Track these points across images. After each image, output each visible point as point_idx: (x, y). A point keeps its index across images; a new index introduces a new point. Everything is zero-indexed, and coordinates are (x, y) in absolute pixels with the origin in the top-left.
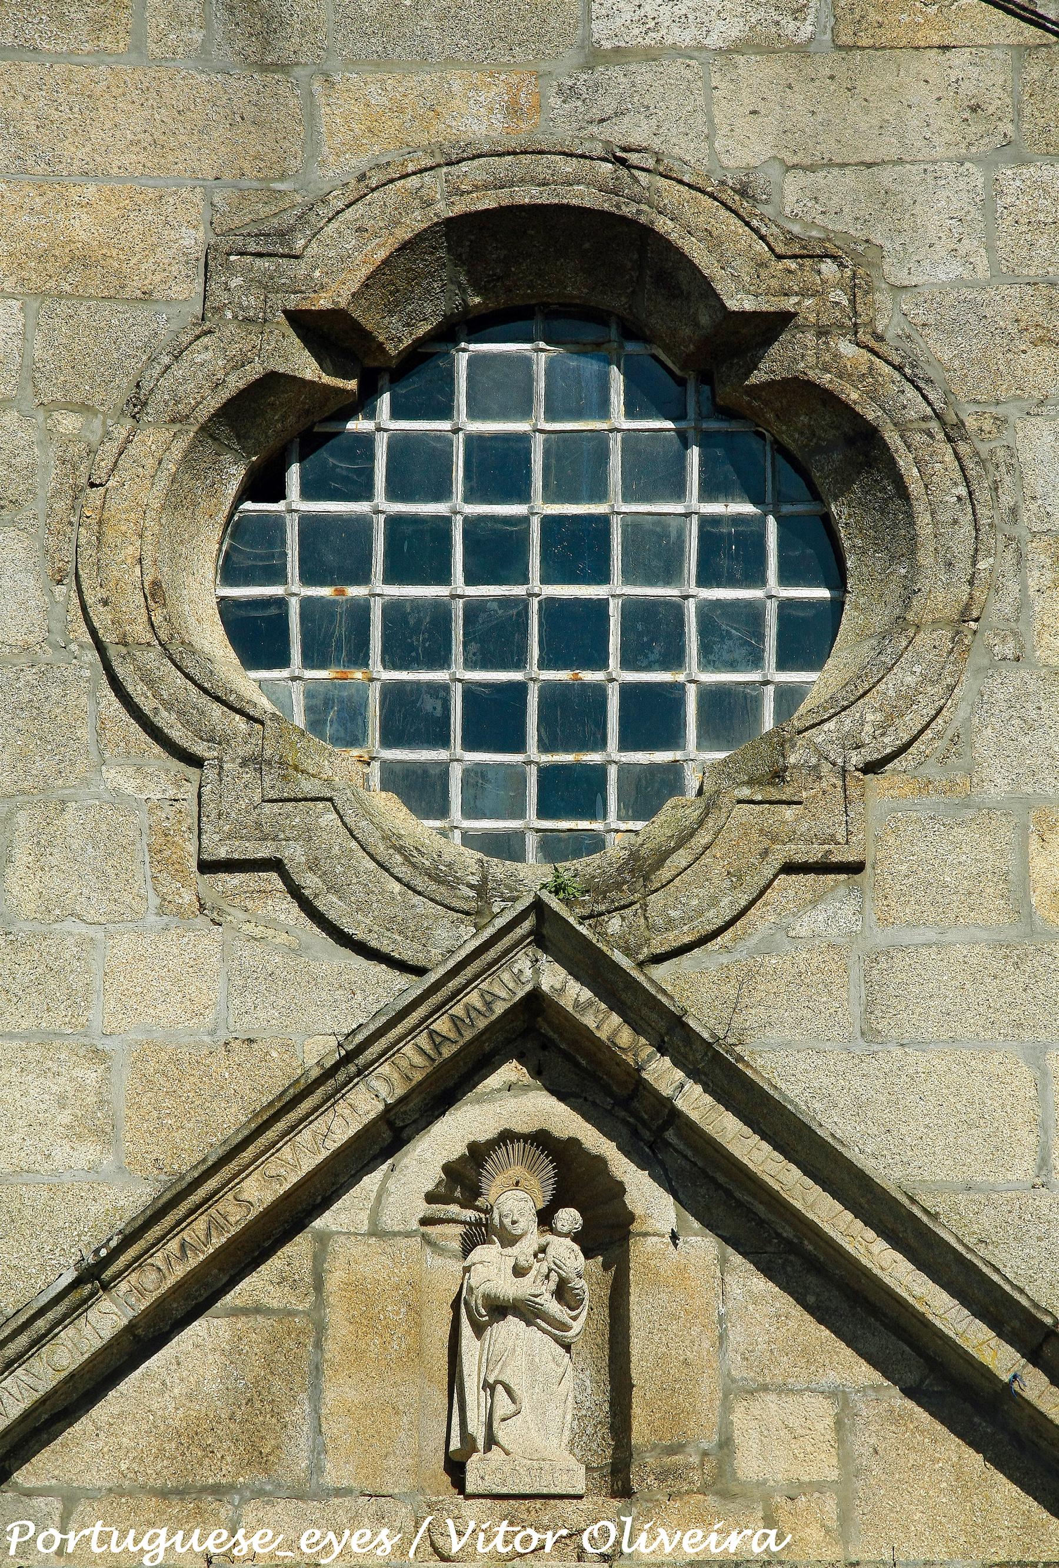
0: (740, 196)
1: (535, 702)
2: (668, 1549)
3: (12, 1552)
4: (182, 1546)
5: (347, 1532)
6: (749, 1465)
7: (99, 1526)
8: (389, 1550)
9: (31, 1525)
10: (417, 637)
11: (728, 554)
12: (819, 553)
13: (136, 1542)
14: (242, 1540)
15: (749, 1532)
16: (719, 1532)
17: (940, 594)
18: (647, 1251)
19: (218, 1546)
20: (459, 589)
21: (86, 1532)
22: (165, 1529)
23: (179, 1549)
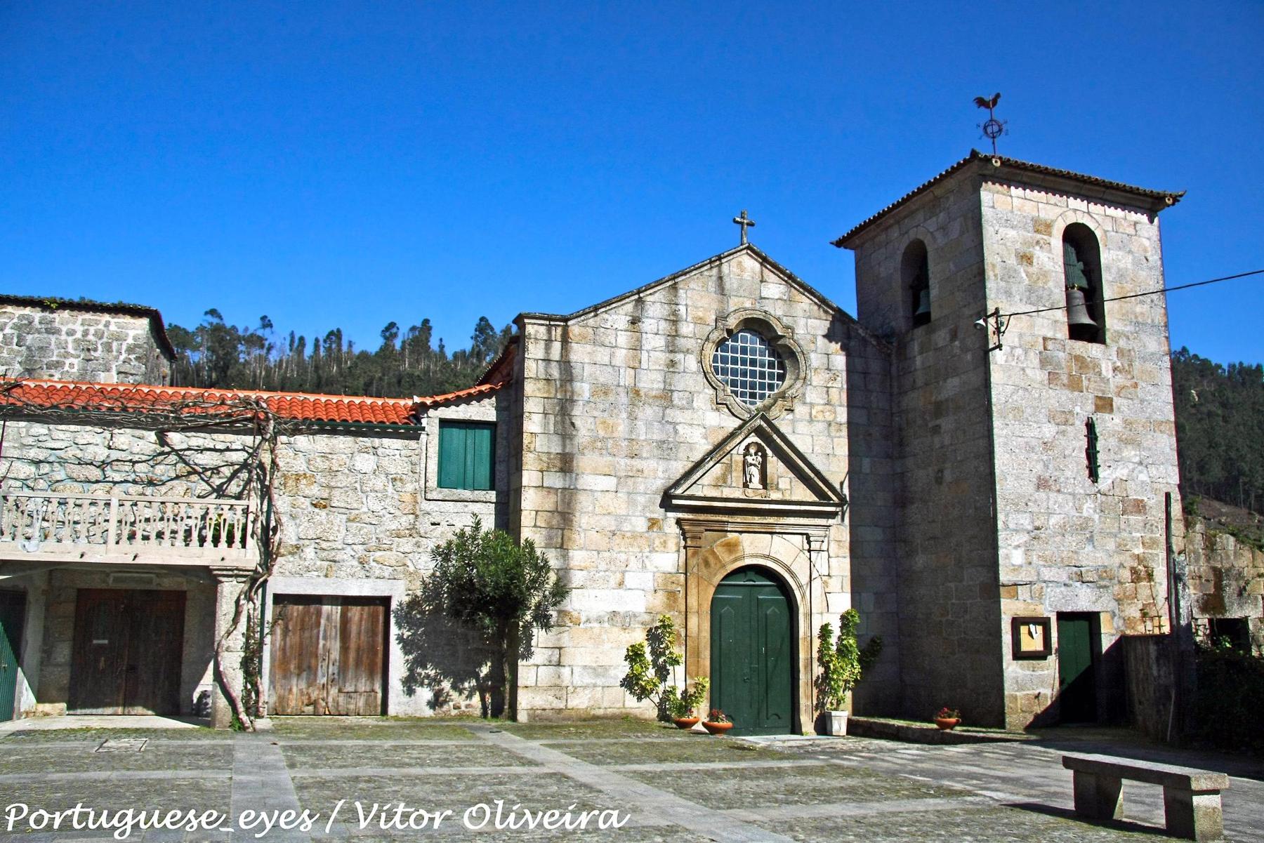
0: (778, 319)
3: (10, 828)
6: (780, 486)
7: (78, 809)
9: (25, 807)
11: (771, 365)
14: (193, 819)
15: (596, 812)
16: (573, 812)
17: (802, 375)
18: (769, 459)
20: (739, 366)
21: (69, 812)
23: (142, 825)
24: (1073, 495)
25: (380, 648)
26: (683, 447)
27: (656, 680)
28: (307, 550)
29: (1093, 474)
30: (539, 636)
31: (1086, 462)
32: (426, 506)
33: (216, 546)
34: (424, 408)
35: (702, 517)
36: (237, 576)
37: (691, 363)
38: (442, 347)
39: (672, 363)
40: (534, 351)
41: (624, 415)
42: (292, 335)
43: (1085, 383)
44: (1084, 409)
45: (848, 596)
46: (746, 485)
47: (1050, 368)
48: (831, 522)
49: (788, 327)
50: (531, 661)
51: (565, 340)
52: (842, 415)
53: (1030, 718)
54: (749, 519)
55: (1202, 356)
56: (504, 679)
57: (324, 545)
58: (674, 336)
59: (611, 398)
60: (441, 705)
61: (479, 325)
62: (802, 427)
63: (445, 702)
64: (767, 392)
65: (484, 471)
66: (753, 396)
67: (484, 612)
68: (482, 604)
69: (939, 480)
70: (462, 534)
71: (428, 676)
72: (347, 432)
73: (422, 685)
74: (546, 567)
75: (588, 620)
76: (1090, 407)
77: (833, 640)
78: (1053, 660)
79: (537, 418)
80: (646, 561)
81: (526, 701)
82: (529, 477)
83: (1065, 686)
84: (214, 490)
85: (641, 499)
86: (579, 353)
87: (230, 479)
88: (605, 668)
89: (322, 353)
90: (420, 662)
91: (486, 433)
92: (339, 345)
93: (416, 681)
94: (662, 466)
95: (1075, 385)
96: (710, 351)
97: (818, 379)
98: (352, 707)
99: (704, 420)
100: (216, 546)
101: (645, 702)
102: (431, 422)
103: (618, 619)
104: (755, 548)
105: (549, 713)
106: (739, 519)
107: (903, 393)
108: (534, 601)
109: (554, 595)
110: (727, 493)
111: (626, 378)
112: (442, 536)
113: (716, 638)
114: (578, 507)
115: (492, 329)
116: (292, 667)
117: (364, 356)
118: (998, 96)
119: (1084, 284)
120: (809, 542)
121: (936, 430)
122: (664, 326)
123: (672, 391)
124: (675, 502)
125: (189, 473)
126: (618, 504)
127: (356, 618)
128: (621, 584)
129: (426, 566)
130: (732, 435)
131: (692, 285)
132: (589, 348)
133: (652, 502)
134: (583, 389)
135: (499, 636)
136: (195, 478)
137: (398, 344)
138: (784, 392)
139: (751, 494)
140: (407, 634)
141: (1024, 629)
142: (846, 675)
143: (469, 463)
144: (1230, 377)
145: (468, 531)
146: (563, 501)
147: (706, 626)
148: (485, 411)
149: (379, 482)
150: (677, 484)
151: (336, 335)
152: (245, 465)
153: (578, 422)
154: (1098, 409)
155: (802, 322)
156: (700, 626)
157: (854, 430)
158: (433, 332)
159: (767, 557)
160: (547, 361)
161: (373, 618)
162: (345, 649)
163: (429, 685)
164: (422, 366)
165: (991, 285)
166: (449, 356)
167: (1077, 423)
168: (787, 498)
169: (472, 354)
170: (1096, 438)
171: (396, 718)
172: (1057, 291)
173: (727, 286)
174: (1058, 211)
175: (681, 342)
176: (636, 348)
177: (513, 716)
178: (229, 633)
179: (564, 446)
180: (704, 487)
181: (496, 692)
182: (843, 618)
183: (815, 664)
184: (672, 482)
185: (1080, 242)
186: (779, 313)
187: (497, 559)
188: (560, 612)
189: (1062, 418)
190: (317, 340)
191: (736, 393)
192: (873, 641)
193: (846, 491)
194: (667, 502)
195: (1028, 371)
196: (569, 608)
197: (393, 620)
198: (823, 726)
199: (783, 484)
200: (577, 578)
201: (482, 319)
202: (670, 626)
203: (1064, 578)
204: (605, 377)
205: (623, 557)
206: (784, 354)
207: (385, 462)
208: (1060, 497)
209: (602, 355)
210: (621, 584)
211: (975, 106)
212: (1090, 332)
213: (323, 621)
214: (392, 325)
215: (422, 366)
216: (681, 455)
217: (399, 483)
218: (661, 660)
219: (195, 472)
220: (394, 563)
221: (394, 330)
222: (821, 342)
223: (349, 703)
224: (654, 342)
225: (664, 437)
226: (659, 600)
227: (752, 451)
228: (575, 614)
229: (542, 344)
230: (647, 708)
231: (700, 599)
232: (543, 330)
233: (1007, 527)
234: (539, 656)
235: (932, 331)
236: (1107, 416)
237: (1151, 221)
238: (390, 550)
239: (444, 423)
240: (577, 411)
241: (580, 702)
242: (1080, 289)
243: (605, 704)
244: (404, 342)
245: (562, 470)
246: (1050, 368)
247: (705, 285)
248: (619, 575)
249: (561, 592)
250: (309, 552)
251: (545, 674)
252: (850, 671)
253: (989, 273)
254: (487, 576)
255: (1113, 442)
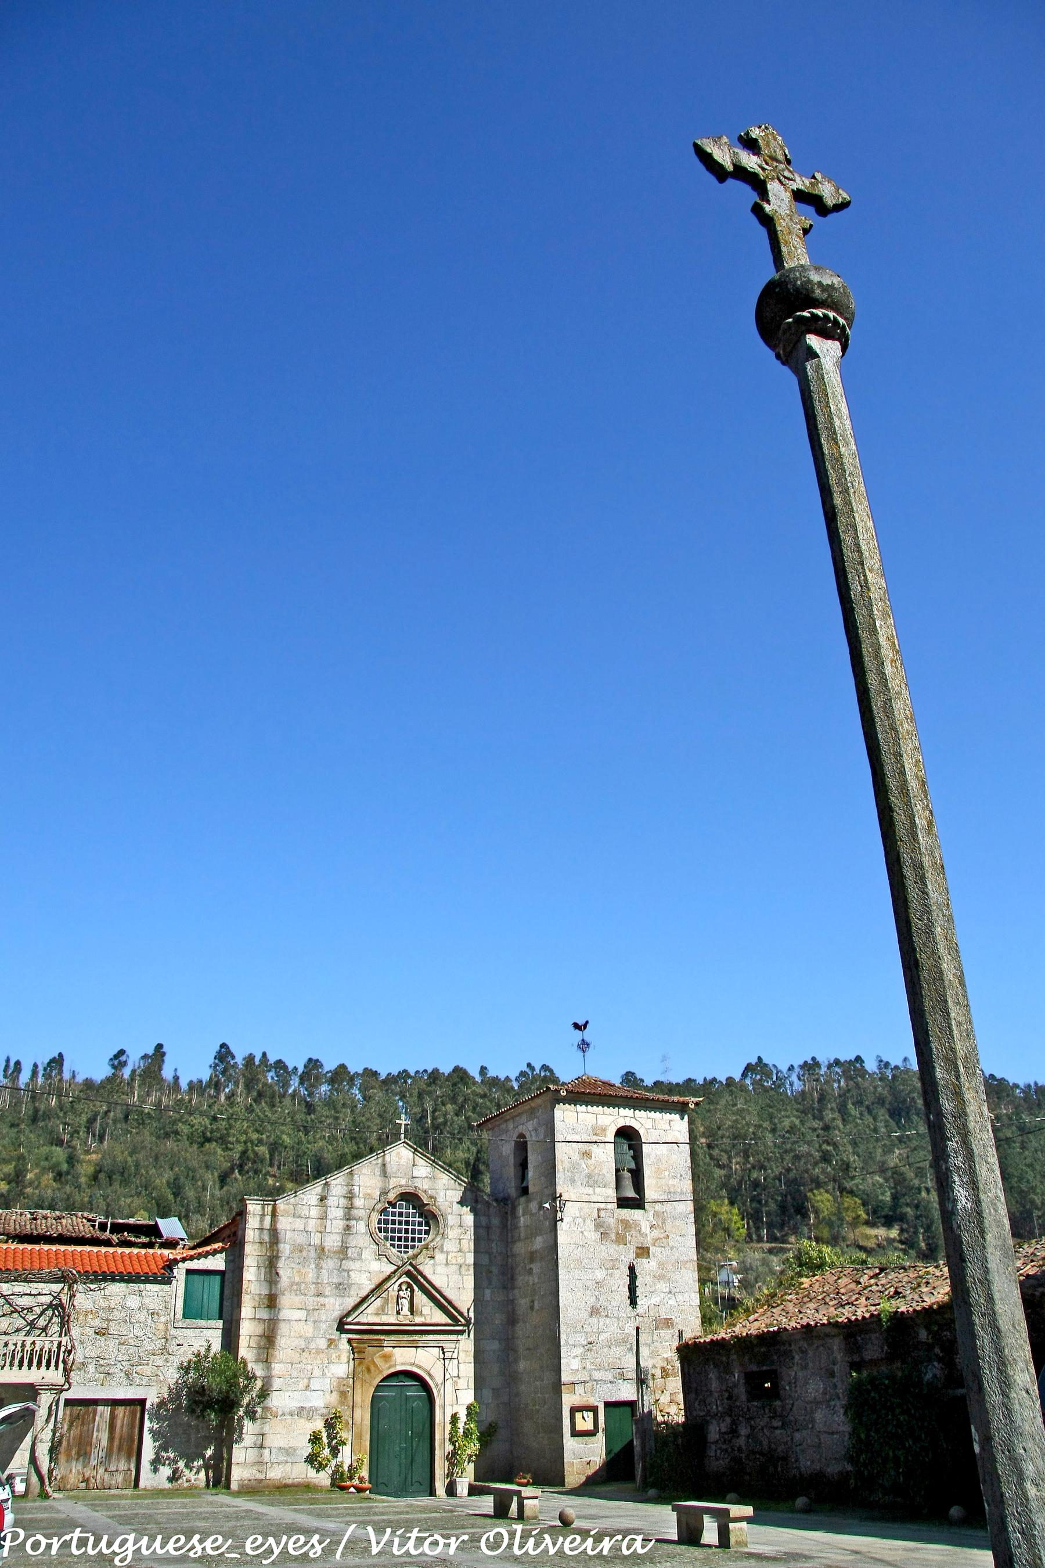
1: (404, 1241)
2: (552, 1551)
4: (162, 1548)
5: (285, 1538)
8: (319, 1552)
10: (393, 1231)
11: (420, 1224)
12: (427, 1224)
13: (109, 1544)
14: (197, 1544)
17: (441, 1231)
19: (176, 1549)
21: (67, 1537)
22: (133, 1535)
23: (144, 1552)
24: (618, 1319)
25: (136, 1437)
26: (354, 1287)
27: (330, 1457)
28: (90, 1366)
29: (633, 1301)
30: (248, 1426)
31: (628, 1294)
32: (173, 1332)
33: (39, 1369)
34: (175, 1262)
35: (366, 1337)
36: (51, 1389)
37: (361, 1227)
38: (176, 1078)
39: (348, 1227)
40: (252, 1223)
41: (313, 1266)
42: (8, 1060)
43: (629, 1238)
44: (627, 1255)
45: (472, 1392)
46: (398, 1313)
47: (602, 1230)
48: (460, 1337)
49: (431, 1197)
50: (242, 1445)
51: (274, 1214)
52: (470, 1259)
53: (584, 1479)
54: (400, 1337)
55: (998, 1076)
56: (223, 1458)
57: (102, 1362)
58: (350, 1208)
59: (304, 1254)
60: (177, 1480)
61: (219, 1052)
62: (440, 1269)
63: (180, 1477)
64: (416, 1244)
65: (215, 1305)
66: (406, 1247)
67: (212, 1408)
68: (209, 1405)
69: (532, 1308)
70: (198, 1355)
71: (169, 1458)
72: (122, 1280)
73: (164, 1465)
74: (254, 1377)
75: (283, 1414)
76: (632, 1256)
77: (461, 1425)
78: (601, 1436)
79: (253, 1270)
80: (326, 1371)
81: (238, 1474)
82: (247, 1311)
83: (612, 1455)
84: (28, 1324)
85: (324, 1326)
86: (284, 1223)
87: (40, 1316)
88: (294, 1449)
89: (40, 1080)
90: (164, 1448)
91: (218, 1278)
92: (61, 1072)
93: (160, 1463)
94: (339, 1300)
95: (621, 1240)
96: (375, 1217)
97: (452, 1234)
98: (113, 1482)
99: (370, 1267)
100: (39, 1369)
101: (322, 1474)
102: (180, 1272)
103: (305, 1413)
104: (403, 1358)
105: (253, 1483)
106: (393, 1337)
107: (514, 1242)
108: (245, 1401)
109: (259, 1397)
110: (385, 1319)
111: (316, 1240)
112: (185, 1355)
113: (375, 1422)
114: (279, 1332)
115: (233, 1057)
116: (73, 1453)
117: (89, 1084)
118: (587, 1022)
119: (633, 1166)
120: (444, 1353)
121: (530, 1272)
122: (343, 1202)
123: (347, 1248)
124: (346, 1327)
125: (12, 1312)
126: (308, 1330)
127: (121, 1415)
128: (308, 1386)
129: (172, 1376)
130: (389, 1278)
131: (364, 1171)
132: (290, 1219)
133: (330, 1326)
134: (285, 1248)
135: (221, 1426)
136: (15, 1315)
137: (126, 1073)
138: (427, 1245)
139: (402, 1319)
140: (156, 1426)
141: (578, 1415)
142: (469, 1452)
143: (205, 1297)
144: (1025, 1099)
145: (203, 1352)
146: (269, 1328)
147: (368, 1416)
148: (218, 1263)
149: (142, 1316)
150: (348, 1314)
151: (58, 1062)
152: (50, 1305)
153: (281, 1272)
154: (638, 1256)
155: (442, 1193)
156: (363, 1416)
157: (479, 1269)
158: (166, 1058)
159: (413, 1364)
160: (261, 1229)
161: (133, 1414)
162: (111, 1439)
163: (169, 1464)
164: (152, 1099)
165: (560, 1176)
166: (184, 1084)
167: (622, 1267)
168: (428, 1321)
169: (209, 1084)
170: (636, 1277)
171: (145, 1489)
172: (609, 1175)
173: (388, 1170)
174: (612, 1118)
175: (354, 1212)
176: (323, 1217)
177: (228, 1486)
178: (43, 1429)
179: (271, 1289)
180: (369, 1316)
181: (217, 1469)
182: (468, 1408)
183: (447, 1443)
184: (345, 1312)
185: (627, 1136)
186: (426, 1187)
187: (221, 1373)
188: (263, 1408)
189: (611, 1265)
190: (35, 1066)
191: (393, 1245)
192: (490, 1425)
193: (472, 1315)
194: (341, 1326)
195: (586, 1233)
196: (270, 1405)
197: (147, 1416)
198: (451, 1491)
199: (426, 1311)
200: (277, 1383)
201: (223, 1046)
202: (340, 1417)
203: (610, 1378)
204: (301, 1239)
205: (309, 1367)
206: (429, 1217)
207: (147, 1301)
208: (608, 1320)
209: (299, 1224)
210: (308, 1386)
211: (572, 1028)
212: (638, 1203)
213: (97, 1418)
214: (122, 1052)
215: (152, 1099)
216: (352, 1293)
217: (156, 1316)
218: (334, 1442)
219: (16, 1311)
220: (150, 1374)
221: (123, 1058)
222: (456, 1207)
223: (111, 1479)
224: (336, 1213)
225: (341, 1280)
226: (334, 1398)
227: (404, 1287)
228: (274, 1409)
229: (258, 1218)
230: (323, 1478)
231: (364, 1397)
232: (259, 1207)
233: (567, 1343)
234: (248, 1440)
235: (529, 1201)
236: (645, 1261)
237: (682, 1119)
238: (148, 1364)
239: (189, 1272)
240: (281, 1264)
241: (275, 1474)
242: (630, 1170)
243: (293, 1476)
244: (134, 1071)
245: (268, 1307)
246: (602, 1230)
247: (373, 1171)
248: (306, 1381)
249: (264, 1394)
250: (91, 1368)
251: (252, 1454)
252: (473, 1447)
253: (559, 1167)
254: (214, 1384)
255: (648, 1279)
